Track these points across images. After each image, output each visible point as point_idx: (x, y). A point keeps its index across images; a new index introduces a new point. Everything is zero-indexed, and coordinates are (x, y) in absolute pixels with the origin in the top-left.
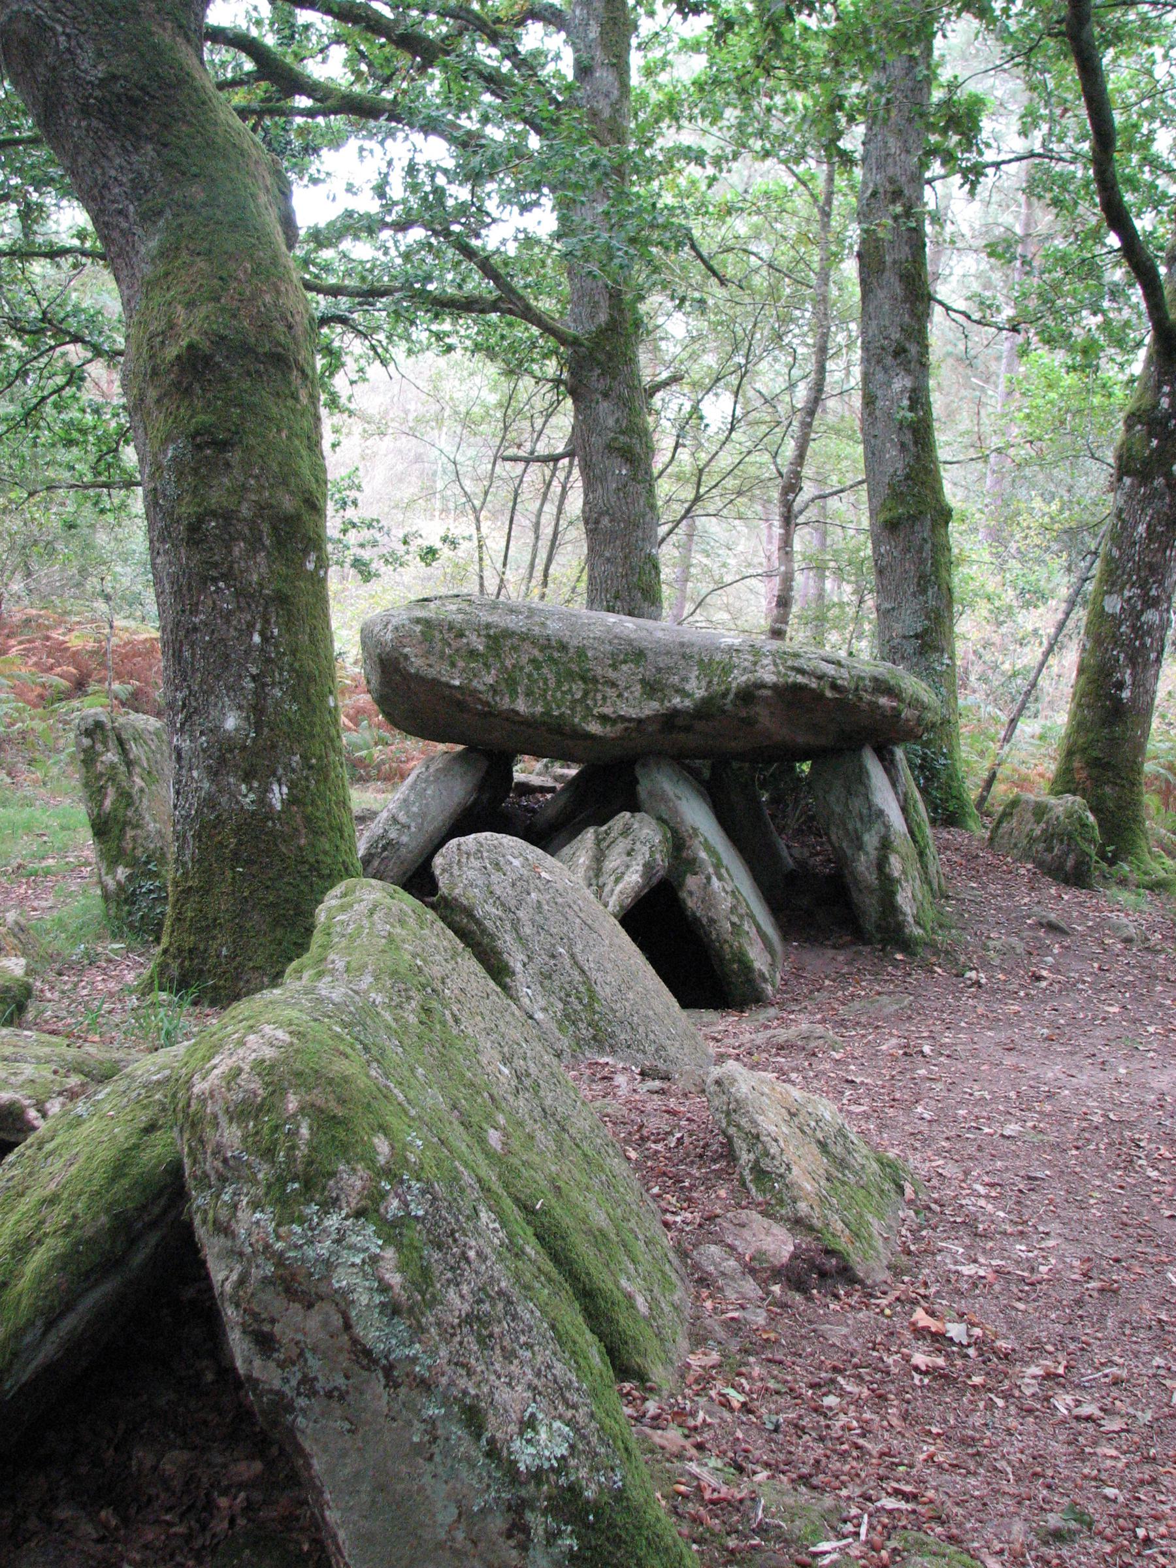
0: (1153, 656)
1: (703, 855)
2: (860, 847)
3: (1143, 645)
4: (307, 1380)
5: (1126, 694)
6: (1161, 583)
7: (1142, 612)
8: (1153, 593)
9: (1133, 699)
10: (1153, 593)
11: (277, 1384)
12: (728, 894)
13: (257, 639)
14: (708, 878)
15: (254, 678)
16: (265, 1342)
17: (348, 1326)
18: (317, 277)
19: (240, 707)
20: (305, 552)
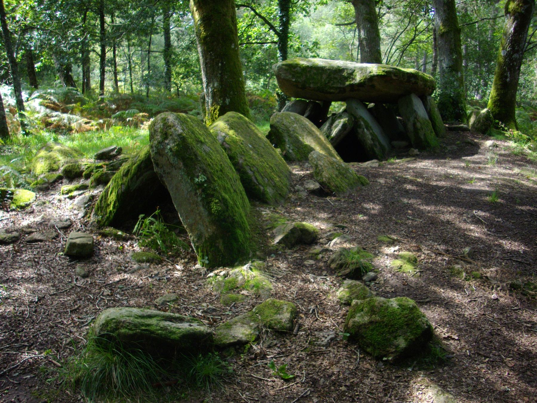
0: (517, 68)
1: (362, 123)
2: (409, 120)
3: (513, 64)
4: (164, 171)
5: (508, 80)
6: (518, 46)
7: (513, 55)
8: (516, 48)
9: (511, 81)
10: (516, 48)
11: (160, 172)
12: (371, 133)
13: (220, 64)
14: (364, 129)
15: (220, 74)
16: (157, 165)
17: (168, 160)
18: (352, 27)
19: (217, 81)
20: (231, 44)
